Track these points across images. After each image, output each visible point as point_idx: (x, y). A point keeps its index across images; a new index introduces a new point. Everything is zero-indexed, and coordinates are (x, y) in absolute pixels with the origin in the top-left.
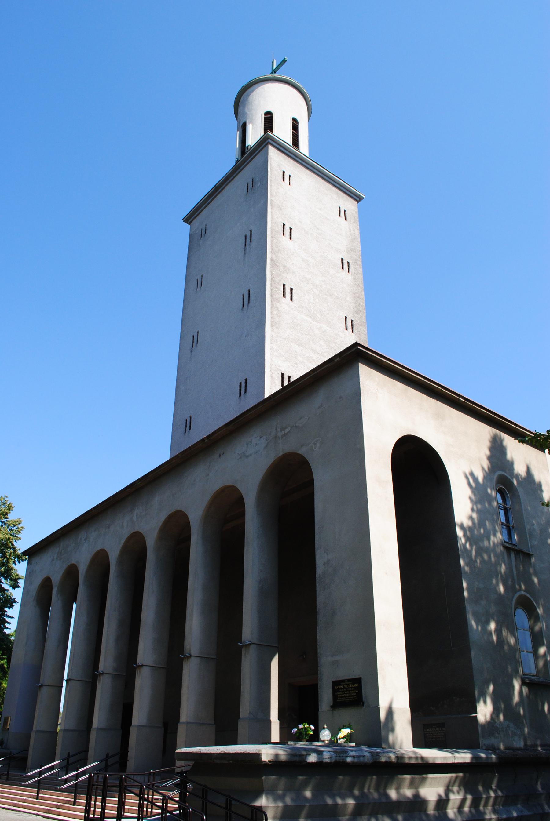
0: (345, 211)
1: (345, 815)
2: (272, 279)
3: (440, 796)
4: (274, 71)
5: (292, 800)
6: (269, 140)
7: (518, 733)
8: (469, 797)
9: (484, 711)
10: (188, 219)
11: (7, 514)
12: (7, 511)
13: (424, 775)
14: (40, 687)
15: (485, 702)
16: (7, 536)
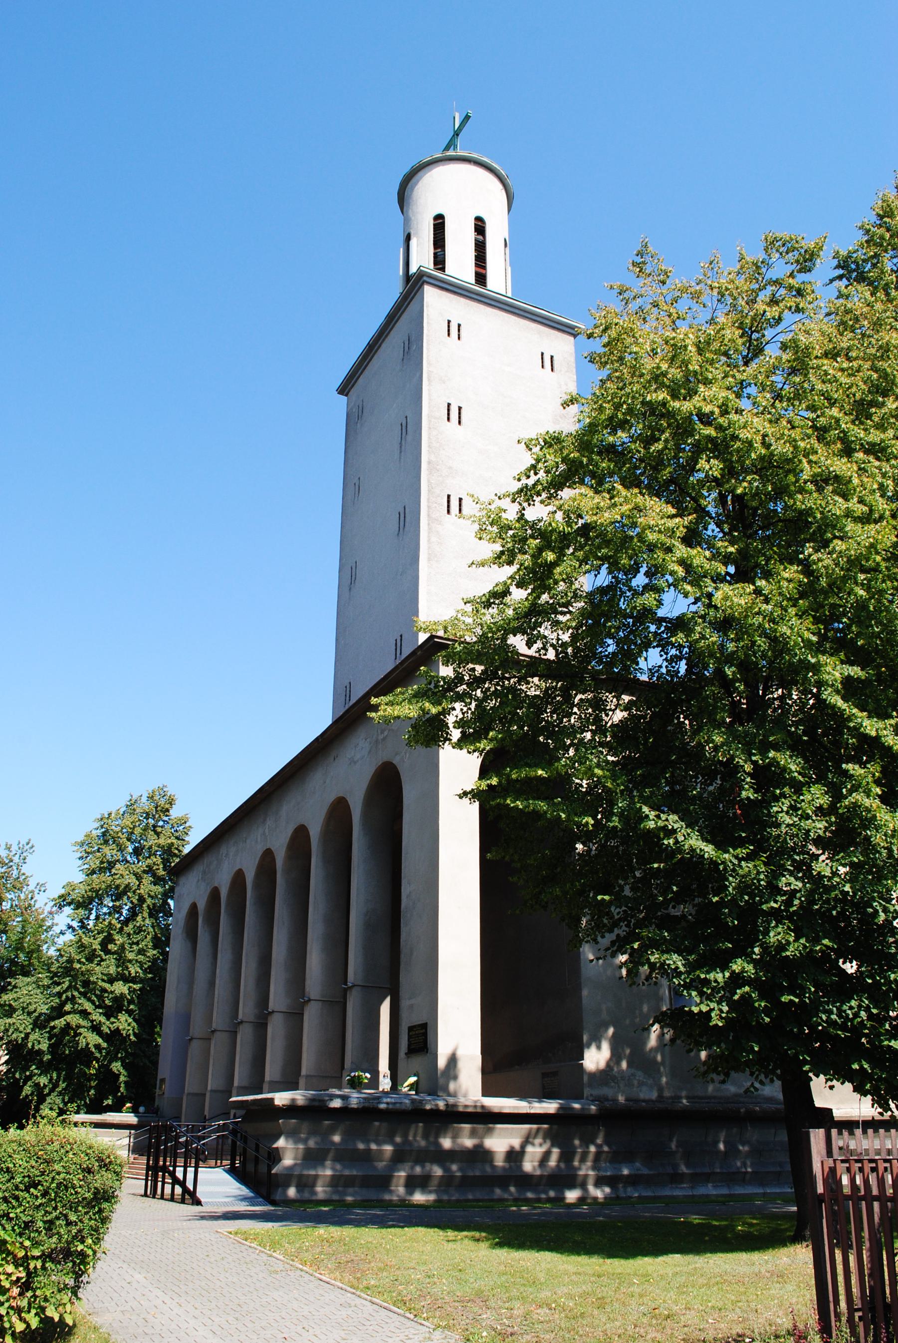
0: (552, 357)
1: (382, 1161)
2: (429, 491)
3: (512, 1148)
4: (451, 144)
5: (316, 1143)
6: (425, 278)
7: (649, 1082)
8: (556, 1151)
9: (595, 1058)
10: (344, 389)
11: (168, 810)
12: (167, 806)
13: (491, 1125)
14: (190, 1040)
15: (599, 1047)
16: (169, 841)
